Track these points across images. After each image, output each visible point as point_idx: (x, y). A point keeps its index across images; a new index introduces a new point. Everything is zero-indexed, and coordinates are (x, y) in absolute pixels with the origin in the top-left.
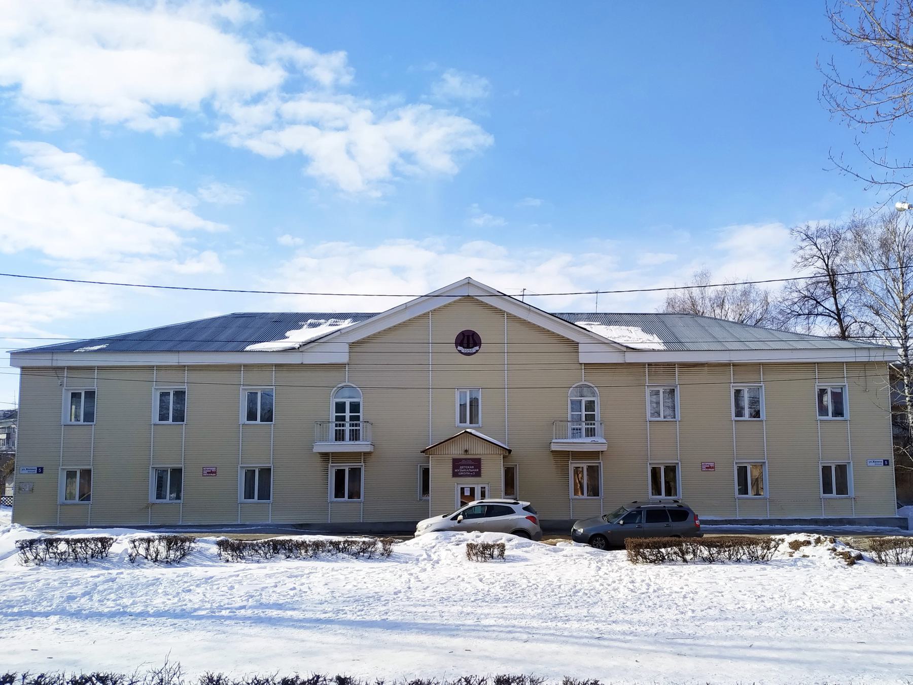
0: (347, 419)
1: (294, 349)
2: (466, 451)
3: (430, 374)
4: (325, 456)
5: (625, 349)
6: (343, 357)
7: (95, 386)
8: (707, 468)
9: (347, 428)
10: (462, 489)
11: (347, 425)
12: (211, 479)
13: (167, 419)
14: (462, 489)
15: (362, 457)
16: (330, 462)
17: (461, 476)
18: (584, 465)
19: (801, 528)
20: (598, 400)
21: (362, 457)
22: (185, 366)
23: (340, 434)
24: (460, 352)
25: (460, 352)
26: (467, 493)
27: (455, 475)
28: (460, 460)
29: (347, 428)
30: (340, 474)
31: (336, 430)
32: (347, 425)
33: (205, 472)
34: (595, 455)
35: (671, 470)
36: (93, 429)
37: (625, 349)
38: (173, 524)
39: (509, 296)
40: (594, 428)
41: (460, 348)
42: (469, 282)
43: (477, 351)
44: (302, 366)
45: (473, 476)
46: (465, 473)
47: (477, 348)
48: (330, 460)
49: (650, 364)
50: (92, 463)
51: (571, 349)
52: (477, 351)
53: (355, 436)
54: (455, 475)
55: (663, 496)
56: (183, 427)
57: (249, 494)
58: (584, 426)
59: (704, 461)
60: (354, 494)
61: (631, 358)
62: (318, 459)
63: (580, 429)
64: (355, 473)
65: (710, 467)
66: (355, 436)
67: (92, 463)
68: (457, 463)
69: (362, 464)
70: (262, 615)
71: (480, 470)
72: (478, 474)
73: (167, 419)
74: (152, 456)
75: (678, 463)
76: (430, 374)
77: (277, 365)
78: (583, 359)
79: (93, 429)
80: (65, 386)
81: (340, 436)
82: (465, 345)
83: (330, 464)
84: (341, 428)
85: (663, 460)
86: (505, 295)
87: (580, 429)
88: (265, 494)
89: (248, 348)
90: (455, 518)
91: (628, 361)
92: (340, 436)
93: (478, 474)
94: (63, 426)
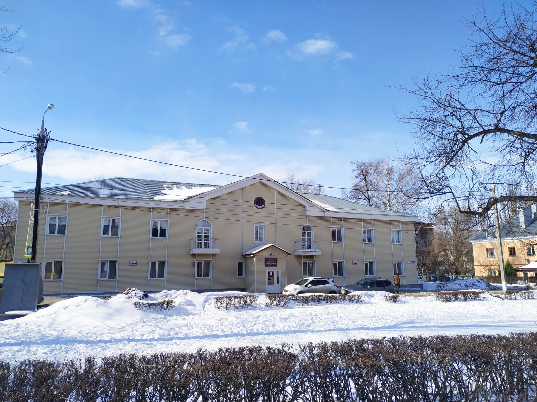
0: (203, 237)
1: (181, 201)
2: (271, 254)
3: (168, 215)
4: (194, 256)
5: (325, 210)
6: (204, 206)
7: (67, 214)
8: (132, 264)
9: (203, 242)
10: (269, 272)
11: (203, 240)
12: (134, 267)
13: (54, 233)
14: (269, 272)
15: (212, 256)
16: (196, 258)
17: (269, 266)
18: (203, 261)
19: (232, 293)
20: (211, 229)
21: (212, 256)
22: (120, 206)
23: (200, 245)
24: (256, 207)
25: (256, 207)
26: (271, 274)
27: (266, 265)
28: (268, 258)
29: (203, 242)
30: (199, 265)
31: (205, 243)
32: (203, 240)
33: (131, 263)
34: (312, 257)
35: (341, 264)
36: (65, 238)
37: (325, 210)
38: (112, 292)
39: (277, 182)
40: (208, 243)
41: (256, 205)
42: (262, 175)
43: (263, 207)
44: (184, 210)
45: (273, 266)
46: (270, 265)
47: (263, 206)
48: (196, 257)
49: (333, 218)
50: (63, 258)
51: (302, 209)
52: (263, 207)
53: (207, 246)
54: (266, 265)
55: (369, 275)
56: (64, 239)
57: (153, 275)
58: (307, 244)
59: (353, 260)
60: (207, 275)
61: (327, 214)
62: (190, 257)
63: (305, 245)
64: (207, 264)
65: (355, 263)
66: (207, 246)
67: (63, 258)
68: (267, 260)
69: (212, 260)
70: (212, 334)
71: (277, 264)
72: (276, 265)
73: (54, 233)
74: (100, 254)
75: (166, 261)
76: (168, 215)
77: (170, 209)
78: (308, 213)
79: (65, 238)
80: (48, 213)
81: (200, 246)
82: (258, 203)
83: (196, 260)
84: (207, 242)
85: (337, 260)
86: (275, 181)
87: (305, 245)
88: (341, 273)
89: (57, 194)
90: (306, 286)
91: (326, 216)
92: (200, 246)
93: (276, 265)
94: (46, 236)
